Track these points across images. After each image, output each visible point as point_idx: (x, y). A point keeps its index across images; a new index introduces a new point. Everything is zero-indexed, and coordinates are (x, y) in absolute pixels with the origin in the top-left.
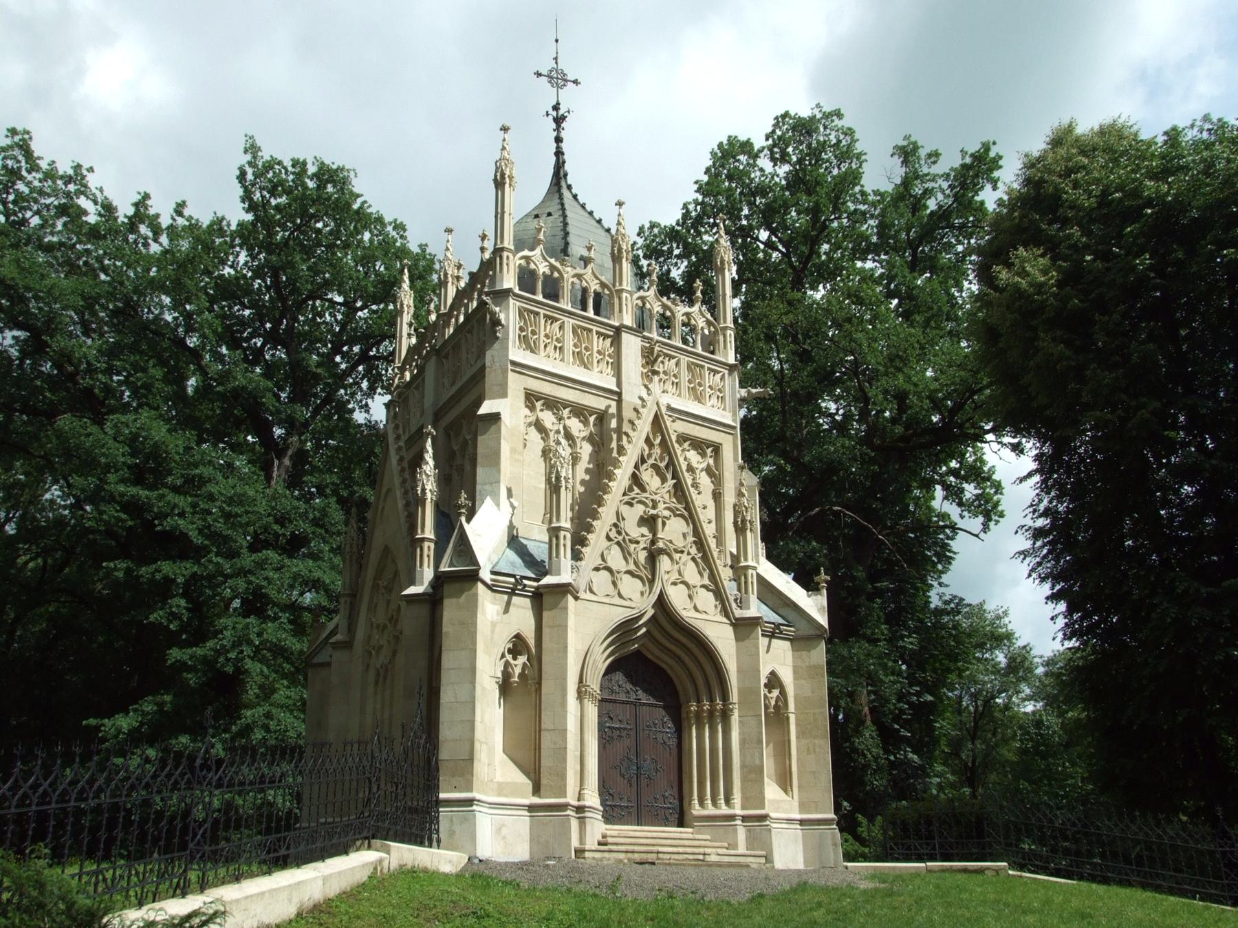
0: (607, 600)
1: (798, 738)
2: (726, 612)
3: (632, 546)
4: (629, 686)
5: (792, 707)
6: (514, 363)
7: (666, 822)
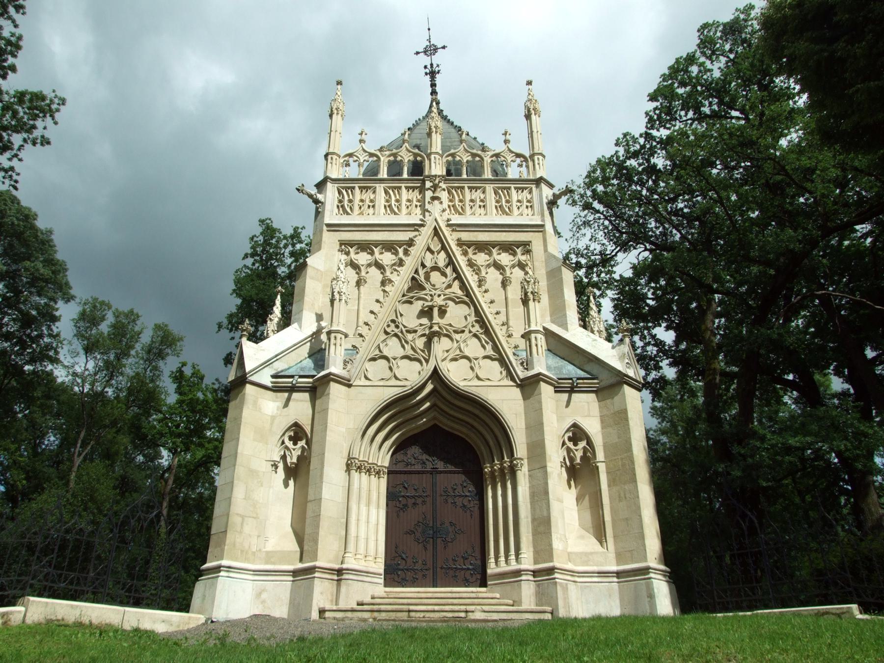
0: (381, 383)
1: (609, 486)
2: (511, 376)
3: (410, 337)
4: (425, 457)
5: (600, 455)
6: (328, 225)
7: (467, 583)
